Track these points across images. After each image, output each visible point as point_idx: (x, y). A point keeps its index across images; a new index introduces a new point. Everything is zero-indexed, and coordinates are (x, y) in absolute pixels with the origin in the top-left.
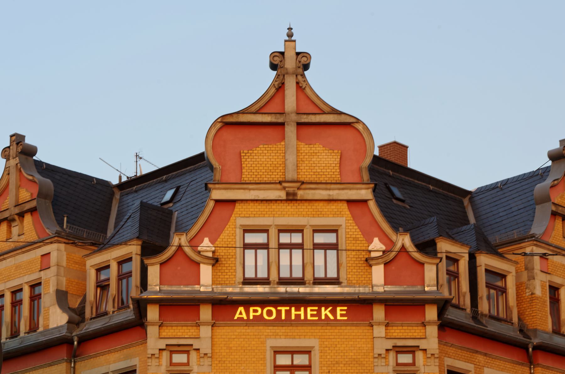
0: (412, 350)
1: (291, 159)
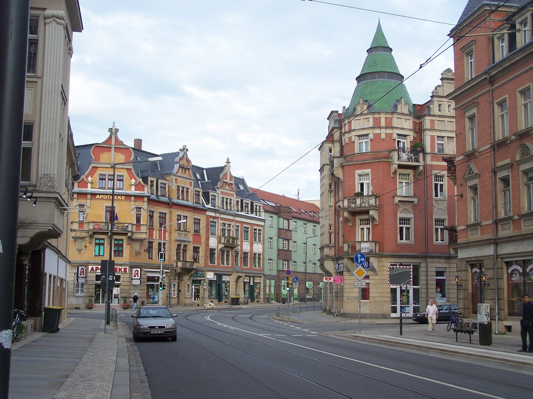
0: (140, 208)
1: (113, 157)
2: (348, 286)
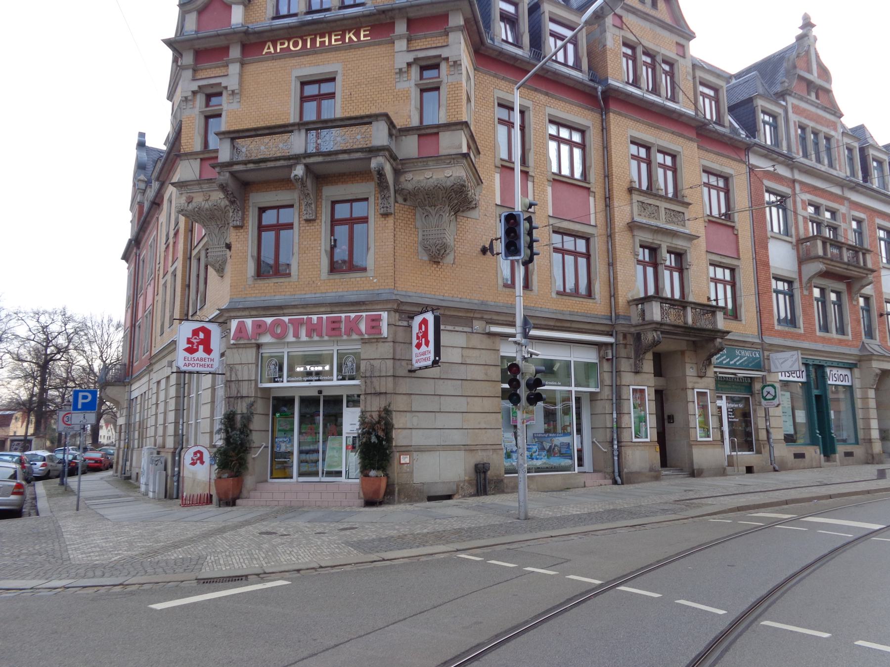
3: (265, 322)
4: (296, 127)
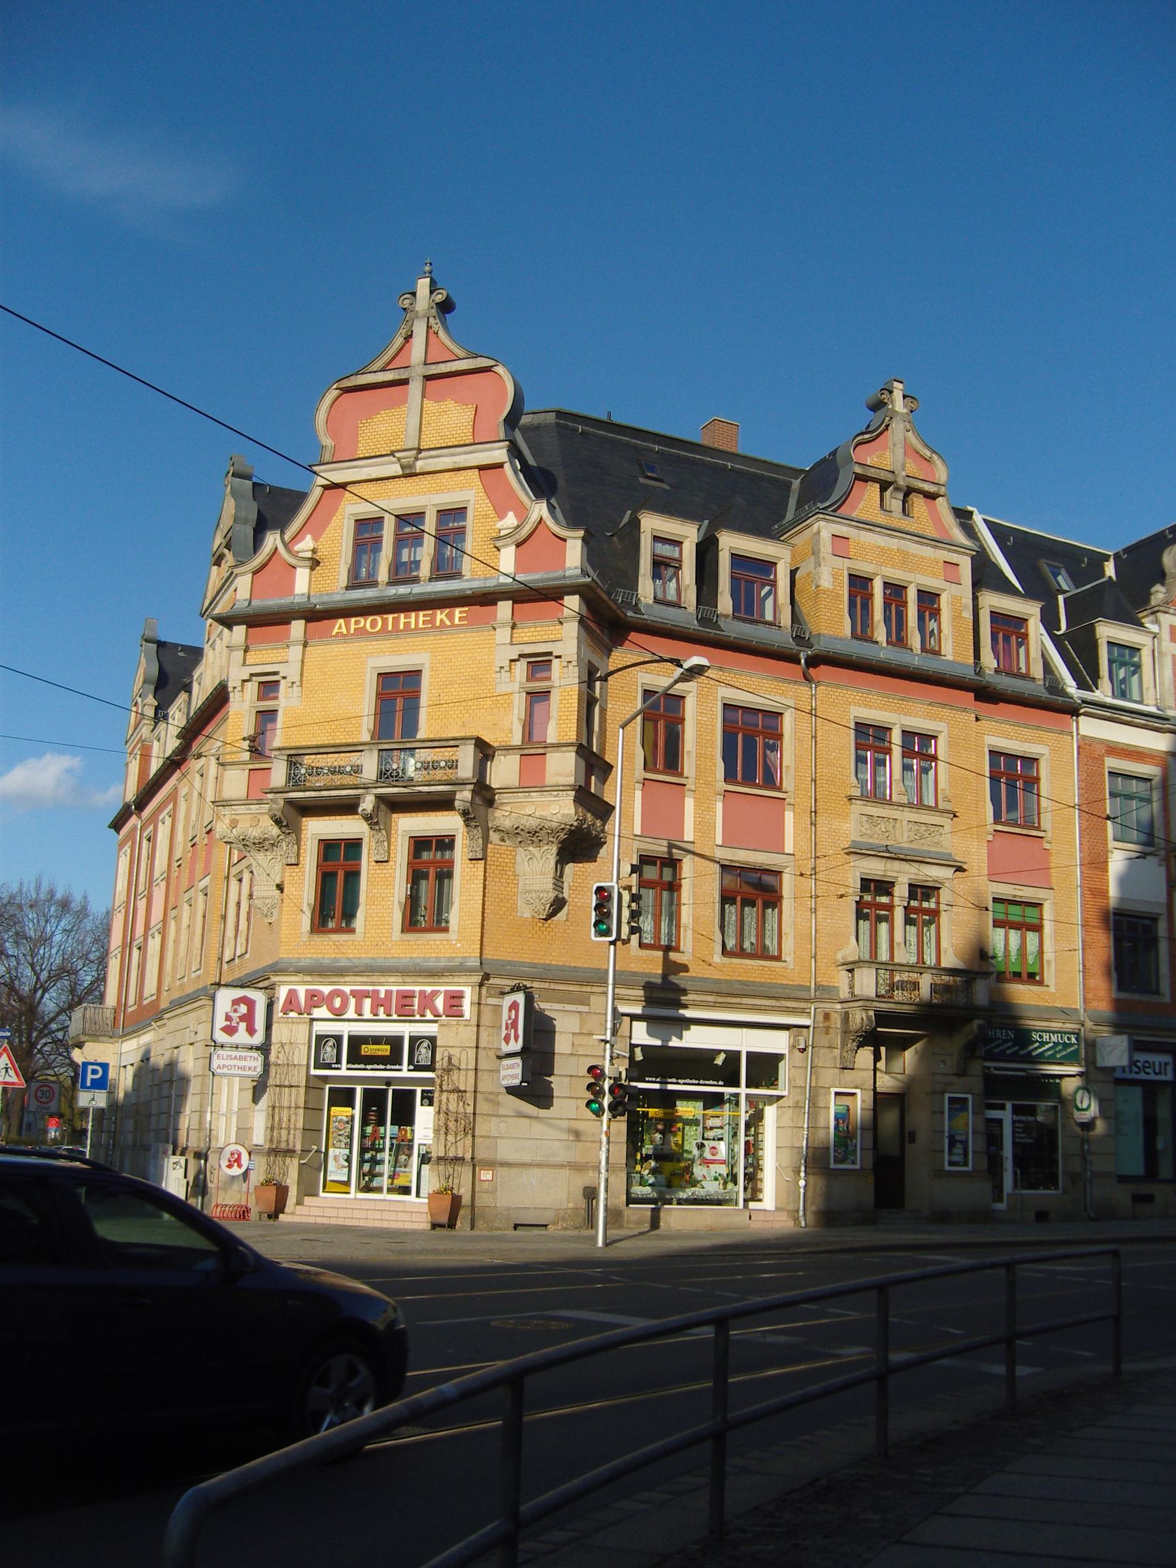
2: (453, 1149)
3: (320, 992)
4: (366, 747)
